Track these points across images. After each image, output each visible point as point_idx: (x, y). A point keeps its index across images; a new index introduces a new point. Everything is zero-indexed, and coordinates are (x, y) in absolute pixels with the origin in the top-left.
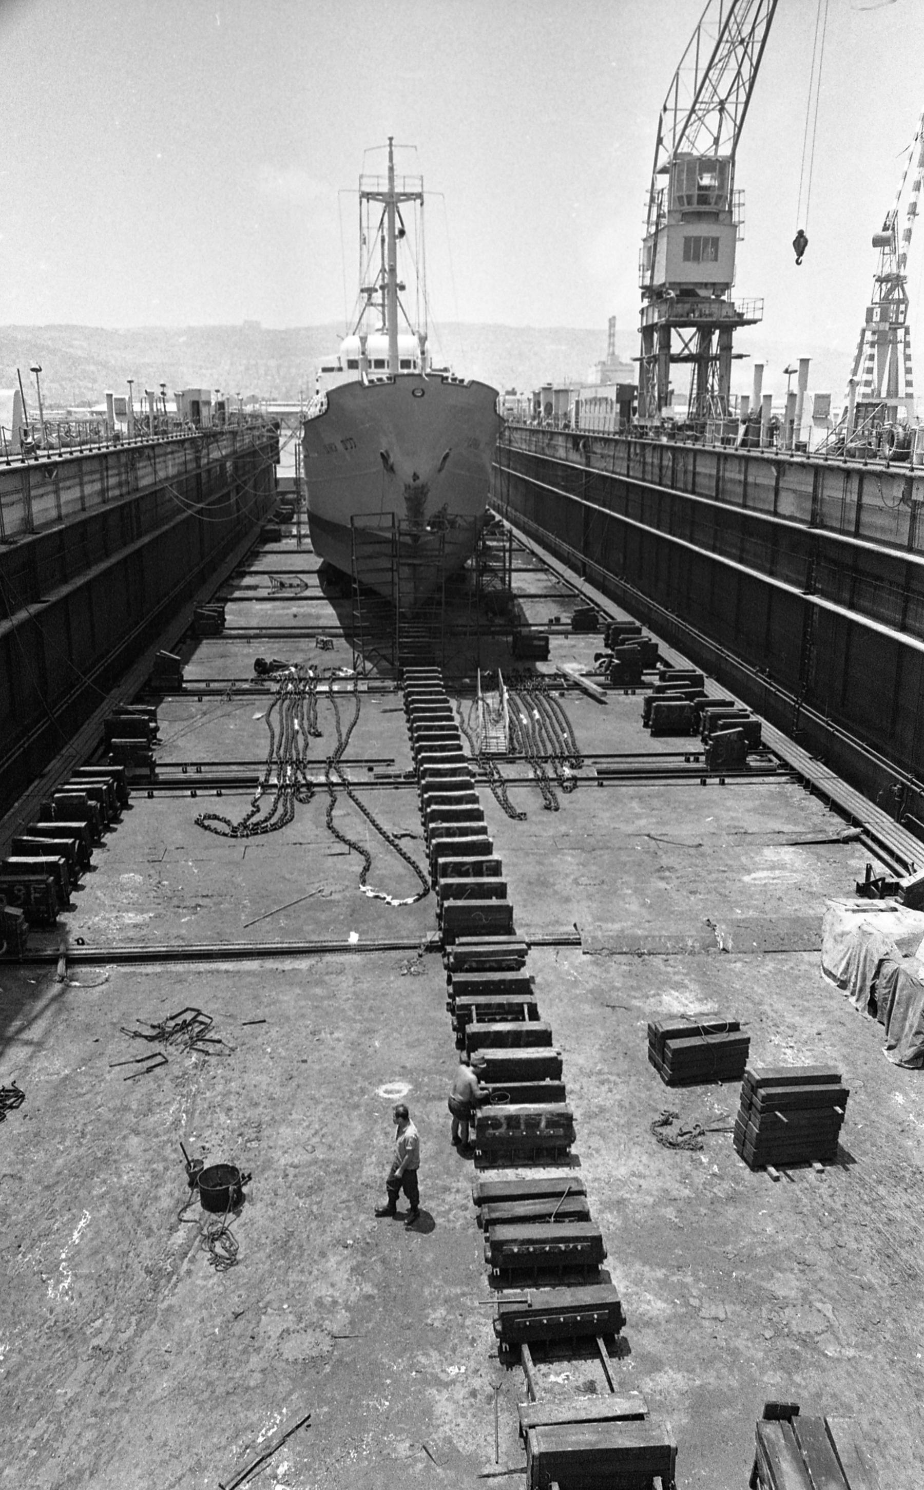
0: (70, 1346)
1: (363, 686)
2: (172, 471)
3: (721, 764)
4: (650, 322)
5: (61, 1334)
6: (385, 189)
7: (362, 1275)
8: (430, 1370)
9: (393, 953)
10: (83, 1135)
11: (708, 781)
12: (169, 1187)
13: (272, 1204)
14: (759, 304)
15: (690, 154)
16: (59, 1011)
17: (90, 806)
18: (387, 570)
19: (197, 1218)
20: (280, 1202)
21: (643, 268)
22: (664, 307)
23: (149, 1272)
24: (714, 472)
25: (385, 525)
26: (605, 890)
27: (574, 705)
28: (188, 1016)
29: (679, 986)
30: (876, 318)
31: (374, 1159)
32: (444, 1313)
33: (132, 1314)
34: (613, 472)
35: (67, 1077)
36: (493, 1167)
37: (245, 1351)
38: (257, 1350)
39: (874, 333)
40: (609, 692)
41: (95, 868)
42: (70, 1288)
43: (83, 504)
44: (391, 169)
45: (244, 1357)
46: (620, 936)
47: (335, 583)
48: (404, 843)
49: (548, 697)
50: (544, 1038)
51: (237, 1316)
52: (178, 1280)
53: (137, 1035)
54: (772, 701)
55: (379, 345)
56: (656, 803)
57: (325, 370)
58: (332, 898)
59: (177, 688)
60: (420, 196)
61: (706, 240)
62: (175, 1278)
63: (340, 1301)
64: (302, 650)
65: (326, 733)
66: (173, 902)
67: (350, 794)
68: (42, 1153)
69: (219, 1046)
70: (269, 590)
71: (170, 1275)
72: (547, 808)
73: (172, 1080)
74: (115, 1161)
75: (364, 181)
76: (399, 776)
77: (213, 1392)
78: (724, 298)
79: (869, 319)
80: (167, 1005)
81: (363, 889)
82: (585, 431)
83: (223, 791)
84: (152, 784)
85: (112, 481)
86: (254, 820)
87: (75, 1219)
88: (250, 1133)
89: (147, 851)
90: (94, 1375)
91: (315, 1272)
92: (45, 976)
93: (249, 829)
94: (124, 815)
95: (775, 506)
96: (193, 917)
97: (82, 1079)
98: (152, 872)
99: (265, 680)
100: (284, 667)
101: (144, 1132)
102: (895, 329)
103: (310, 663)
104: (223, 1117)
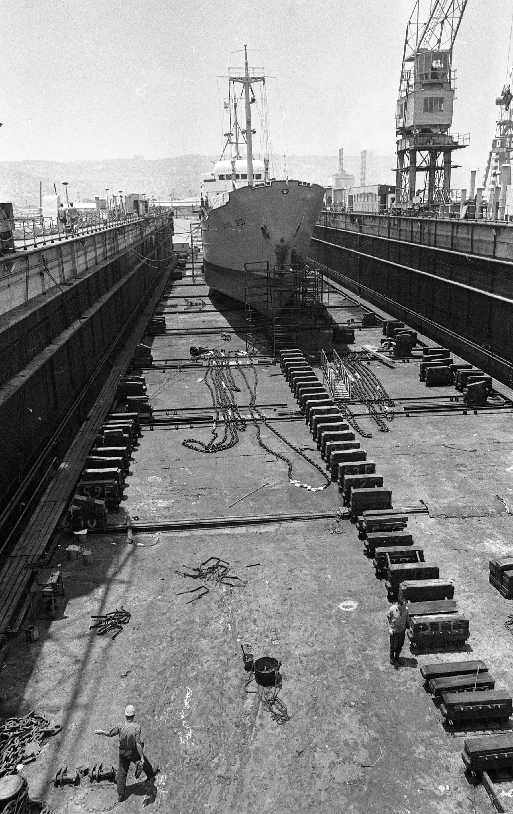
0: (204, 775)
1: (255, 361)
2: (131, 241)
3: (472, 402)
4: (403, 148)
5: (196, 767)
6: (243, 75)
7: (367, 725)
8: (428, 788)
9: (322, 521)
10: (172, 639)
11: (468, 412)
12: (233, 671)
13: (299, 680)
14: (467, 136)
15: (427, 49)
16: (135, 562)
17: (125, 437)
18: (264, 294)
19: (256, 690)
20: (304, 679)
21: (400, 116)
22: (412, 140)
23: (238, 726)
24: (450, 234)
25: (263, 268)
26: (430, 480)
27: (376, 369)
28: (214, 563)
29: (491, 536)
30: (498, 146)
31: (350, 650)
32: (424, 749)
33: (235, 753)
34: (378, 236)
35: (151, 602)
36: (423, 654)
37: (311, 778)
38: (319, 776)
39: (497, 154)
40: (396, 361)
41: (132, 474)
42: (193, 738)
43: (96, 260)
44: (246, 64)
45: (312, 781)
46: (450, 506)
47: (221, 301)
48: (306, 453)
49: (361, 365)
50: (434, 573)
51: (300, 753)
52: (257, 731)
53: (186, 575)
54: (493, 365)
55: (242, 166)
56: (442, 426)
57: (205, 181)
58: (275, 487)
59: (149, 365)
60: (263, 79)
61: (436, 99)
62: (254, 729)
63: (359, 742)
64: (213, 342)
65: (241, 389)
66: (183, 492)
67: (267, 425)
68: (151, 652)
69: (237, 580)
70: (185, 307)
71: (251, 727)
72: (382, 430)
73: (215, 603)
74: (196, 655)
75: (231, 70)
76: (292, 414)
77: (300, 805)
78: (446, 133)
79: (494, 146)
80: (198, 555)
81: (292, 482)
82: (356, 212)
83: (194, 425)
84: (152, 422)
85: (108, 247)
86: (216, 442)
87: (182, 694)
88: (272, 635)
89: (159, 462)
90: (224, 794)
91: (338, 724)
92: (120, 540)
93: (212, 448)
94: (139, 441)
95: (494, 253)
96: (198, 502)
97: (161, 604)
98: (165, 475)
99: (197, 359)
100: (207, 351)
101: (208, 636)
102: (509, 152)
103: (221, 348)
104: (253, 626)
